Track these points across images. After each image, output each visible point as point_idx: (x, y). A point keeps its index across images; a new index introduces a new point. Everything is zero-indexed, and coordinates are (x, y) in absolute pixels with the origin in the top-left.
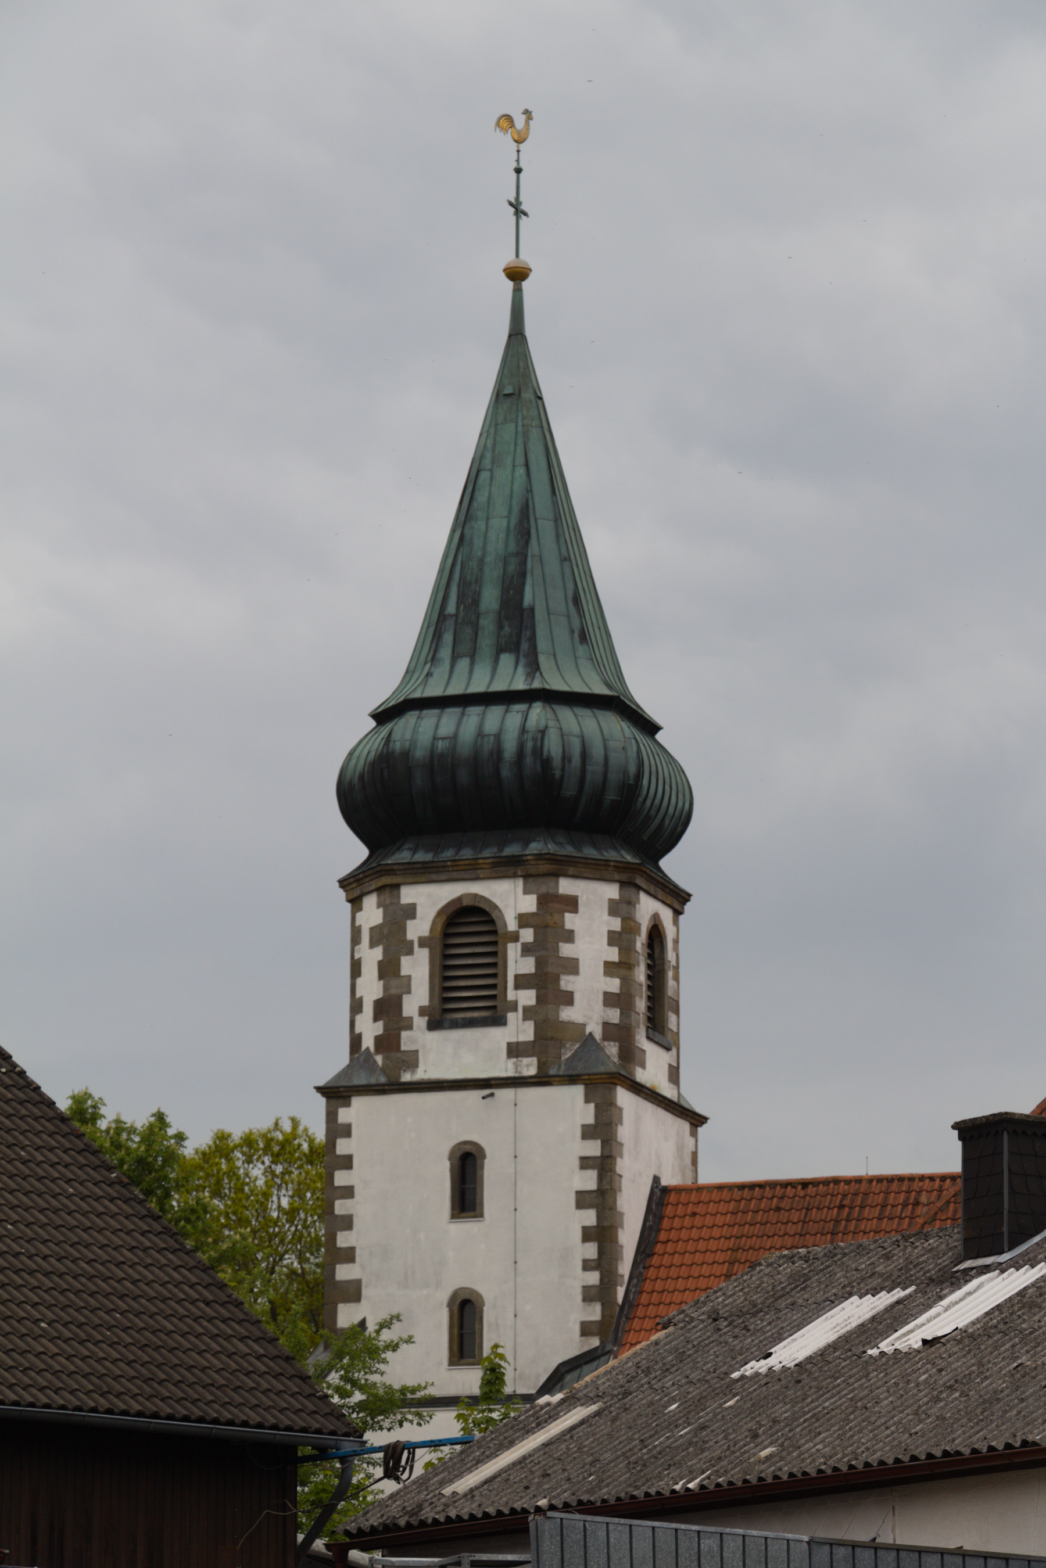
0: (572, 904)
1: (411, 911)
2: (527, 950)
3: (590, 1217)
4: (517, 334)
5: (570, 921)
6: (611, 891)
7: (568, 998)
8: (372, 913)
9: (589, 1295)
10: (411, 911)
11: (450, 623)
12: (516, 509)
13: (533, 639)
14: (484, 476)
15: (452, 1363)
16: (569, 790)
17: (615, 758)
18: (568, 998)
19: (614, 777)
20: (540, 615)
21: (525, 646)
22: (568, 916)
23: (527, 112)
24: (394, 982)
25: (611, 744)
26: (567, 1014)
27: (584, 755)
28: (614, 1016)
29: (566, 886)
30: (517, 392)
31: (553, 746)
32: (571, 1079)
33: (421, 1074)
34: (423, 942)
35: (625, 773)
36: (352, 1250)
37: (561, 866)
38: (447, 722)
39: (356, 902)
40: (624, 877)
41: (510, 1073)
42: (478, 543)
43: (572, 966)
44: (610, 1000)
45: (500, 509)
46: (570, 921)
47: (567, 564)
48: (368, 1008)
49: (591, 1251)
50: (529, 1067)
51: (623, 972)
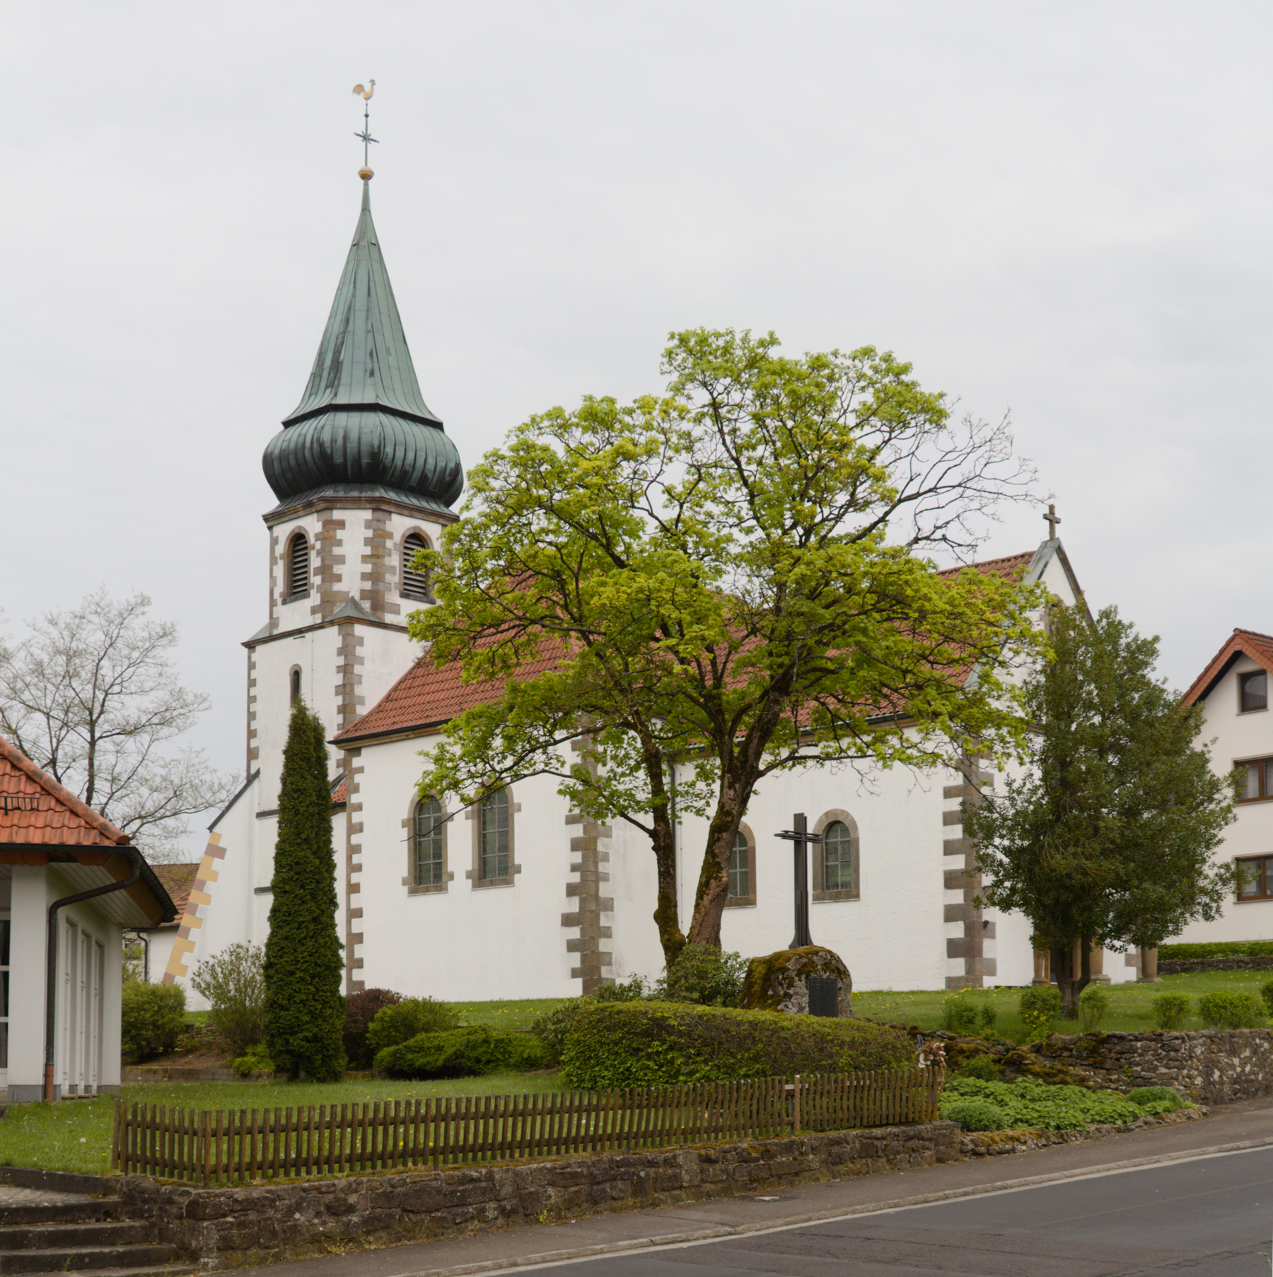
4: (366, 209)
6: (368, 514)
7: (338, 578)
16: (338, 460)
17: (365, 439)
18: (338, 578)
19: (365, 449)
20: (345, 365)
22: (338, 532)
23: (373, 82)
25: (364, 430)
26: (337, 587)
27: (345, 438)
28: (368, 585)
29: (337, 515)
30: (365, 245)
31: (326, 437)
35: (372, 446)
37: (331, 504)
40: (373, 506)
43: (341, 560)
46: (340, 534)
47: (370, 335)
51: (374, 560)
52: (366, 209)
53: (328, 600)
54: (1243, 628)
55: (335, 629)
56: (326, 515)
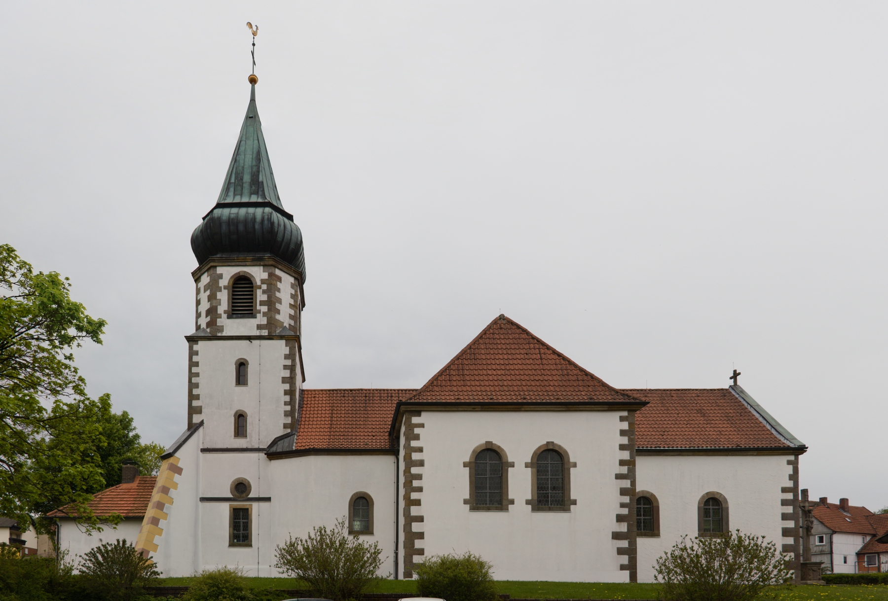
0: (279, 279)
1: (221, 276)
2: (264, 292)
3: (287, 387)
4: (253, 100)
5: (279, 285)
8: (205, 279)
9: (286, 414)
10: (221, 276)
11: (233, 185)
12: (255, 152)
13: (263, 191)
14: (243, 143)
15: (235, 436)
16: (279, 238)
18: (278, 312)
21: (260, 193)
24: (214, 301)
32: (281, 337)
33: (224, 334)
34: (225, 288)
36: (199, 395)
38: (234, 210)
39: (197, 280)
41: (258, 334)
42: (242, 162)
44: (291, 317)
45: (249, 152)
48: (203, 314)
49: (287, 398)
50: (265, 333)
52: (253, 100)
53: (272, 323)
54: (464, 490)
55: (283, 342)
56: (271, 269)
